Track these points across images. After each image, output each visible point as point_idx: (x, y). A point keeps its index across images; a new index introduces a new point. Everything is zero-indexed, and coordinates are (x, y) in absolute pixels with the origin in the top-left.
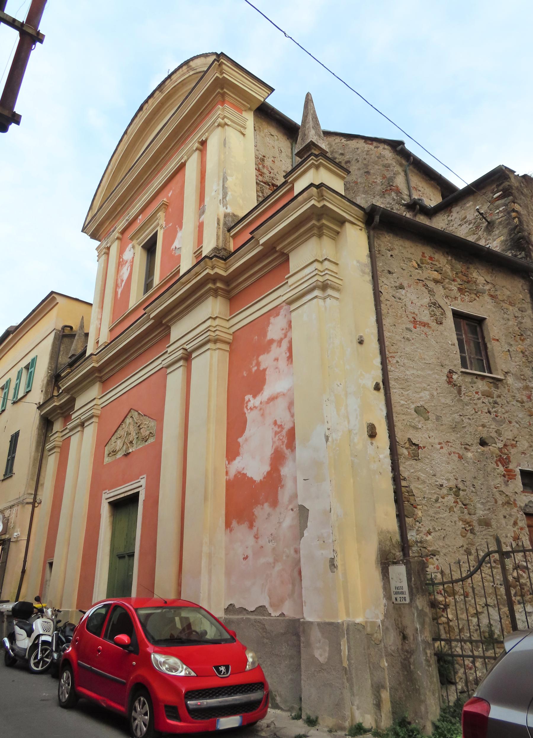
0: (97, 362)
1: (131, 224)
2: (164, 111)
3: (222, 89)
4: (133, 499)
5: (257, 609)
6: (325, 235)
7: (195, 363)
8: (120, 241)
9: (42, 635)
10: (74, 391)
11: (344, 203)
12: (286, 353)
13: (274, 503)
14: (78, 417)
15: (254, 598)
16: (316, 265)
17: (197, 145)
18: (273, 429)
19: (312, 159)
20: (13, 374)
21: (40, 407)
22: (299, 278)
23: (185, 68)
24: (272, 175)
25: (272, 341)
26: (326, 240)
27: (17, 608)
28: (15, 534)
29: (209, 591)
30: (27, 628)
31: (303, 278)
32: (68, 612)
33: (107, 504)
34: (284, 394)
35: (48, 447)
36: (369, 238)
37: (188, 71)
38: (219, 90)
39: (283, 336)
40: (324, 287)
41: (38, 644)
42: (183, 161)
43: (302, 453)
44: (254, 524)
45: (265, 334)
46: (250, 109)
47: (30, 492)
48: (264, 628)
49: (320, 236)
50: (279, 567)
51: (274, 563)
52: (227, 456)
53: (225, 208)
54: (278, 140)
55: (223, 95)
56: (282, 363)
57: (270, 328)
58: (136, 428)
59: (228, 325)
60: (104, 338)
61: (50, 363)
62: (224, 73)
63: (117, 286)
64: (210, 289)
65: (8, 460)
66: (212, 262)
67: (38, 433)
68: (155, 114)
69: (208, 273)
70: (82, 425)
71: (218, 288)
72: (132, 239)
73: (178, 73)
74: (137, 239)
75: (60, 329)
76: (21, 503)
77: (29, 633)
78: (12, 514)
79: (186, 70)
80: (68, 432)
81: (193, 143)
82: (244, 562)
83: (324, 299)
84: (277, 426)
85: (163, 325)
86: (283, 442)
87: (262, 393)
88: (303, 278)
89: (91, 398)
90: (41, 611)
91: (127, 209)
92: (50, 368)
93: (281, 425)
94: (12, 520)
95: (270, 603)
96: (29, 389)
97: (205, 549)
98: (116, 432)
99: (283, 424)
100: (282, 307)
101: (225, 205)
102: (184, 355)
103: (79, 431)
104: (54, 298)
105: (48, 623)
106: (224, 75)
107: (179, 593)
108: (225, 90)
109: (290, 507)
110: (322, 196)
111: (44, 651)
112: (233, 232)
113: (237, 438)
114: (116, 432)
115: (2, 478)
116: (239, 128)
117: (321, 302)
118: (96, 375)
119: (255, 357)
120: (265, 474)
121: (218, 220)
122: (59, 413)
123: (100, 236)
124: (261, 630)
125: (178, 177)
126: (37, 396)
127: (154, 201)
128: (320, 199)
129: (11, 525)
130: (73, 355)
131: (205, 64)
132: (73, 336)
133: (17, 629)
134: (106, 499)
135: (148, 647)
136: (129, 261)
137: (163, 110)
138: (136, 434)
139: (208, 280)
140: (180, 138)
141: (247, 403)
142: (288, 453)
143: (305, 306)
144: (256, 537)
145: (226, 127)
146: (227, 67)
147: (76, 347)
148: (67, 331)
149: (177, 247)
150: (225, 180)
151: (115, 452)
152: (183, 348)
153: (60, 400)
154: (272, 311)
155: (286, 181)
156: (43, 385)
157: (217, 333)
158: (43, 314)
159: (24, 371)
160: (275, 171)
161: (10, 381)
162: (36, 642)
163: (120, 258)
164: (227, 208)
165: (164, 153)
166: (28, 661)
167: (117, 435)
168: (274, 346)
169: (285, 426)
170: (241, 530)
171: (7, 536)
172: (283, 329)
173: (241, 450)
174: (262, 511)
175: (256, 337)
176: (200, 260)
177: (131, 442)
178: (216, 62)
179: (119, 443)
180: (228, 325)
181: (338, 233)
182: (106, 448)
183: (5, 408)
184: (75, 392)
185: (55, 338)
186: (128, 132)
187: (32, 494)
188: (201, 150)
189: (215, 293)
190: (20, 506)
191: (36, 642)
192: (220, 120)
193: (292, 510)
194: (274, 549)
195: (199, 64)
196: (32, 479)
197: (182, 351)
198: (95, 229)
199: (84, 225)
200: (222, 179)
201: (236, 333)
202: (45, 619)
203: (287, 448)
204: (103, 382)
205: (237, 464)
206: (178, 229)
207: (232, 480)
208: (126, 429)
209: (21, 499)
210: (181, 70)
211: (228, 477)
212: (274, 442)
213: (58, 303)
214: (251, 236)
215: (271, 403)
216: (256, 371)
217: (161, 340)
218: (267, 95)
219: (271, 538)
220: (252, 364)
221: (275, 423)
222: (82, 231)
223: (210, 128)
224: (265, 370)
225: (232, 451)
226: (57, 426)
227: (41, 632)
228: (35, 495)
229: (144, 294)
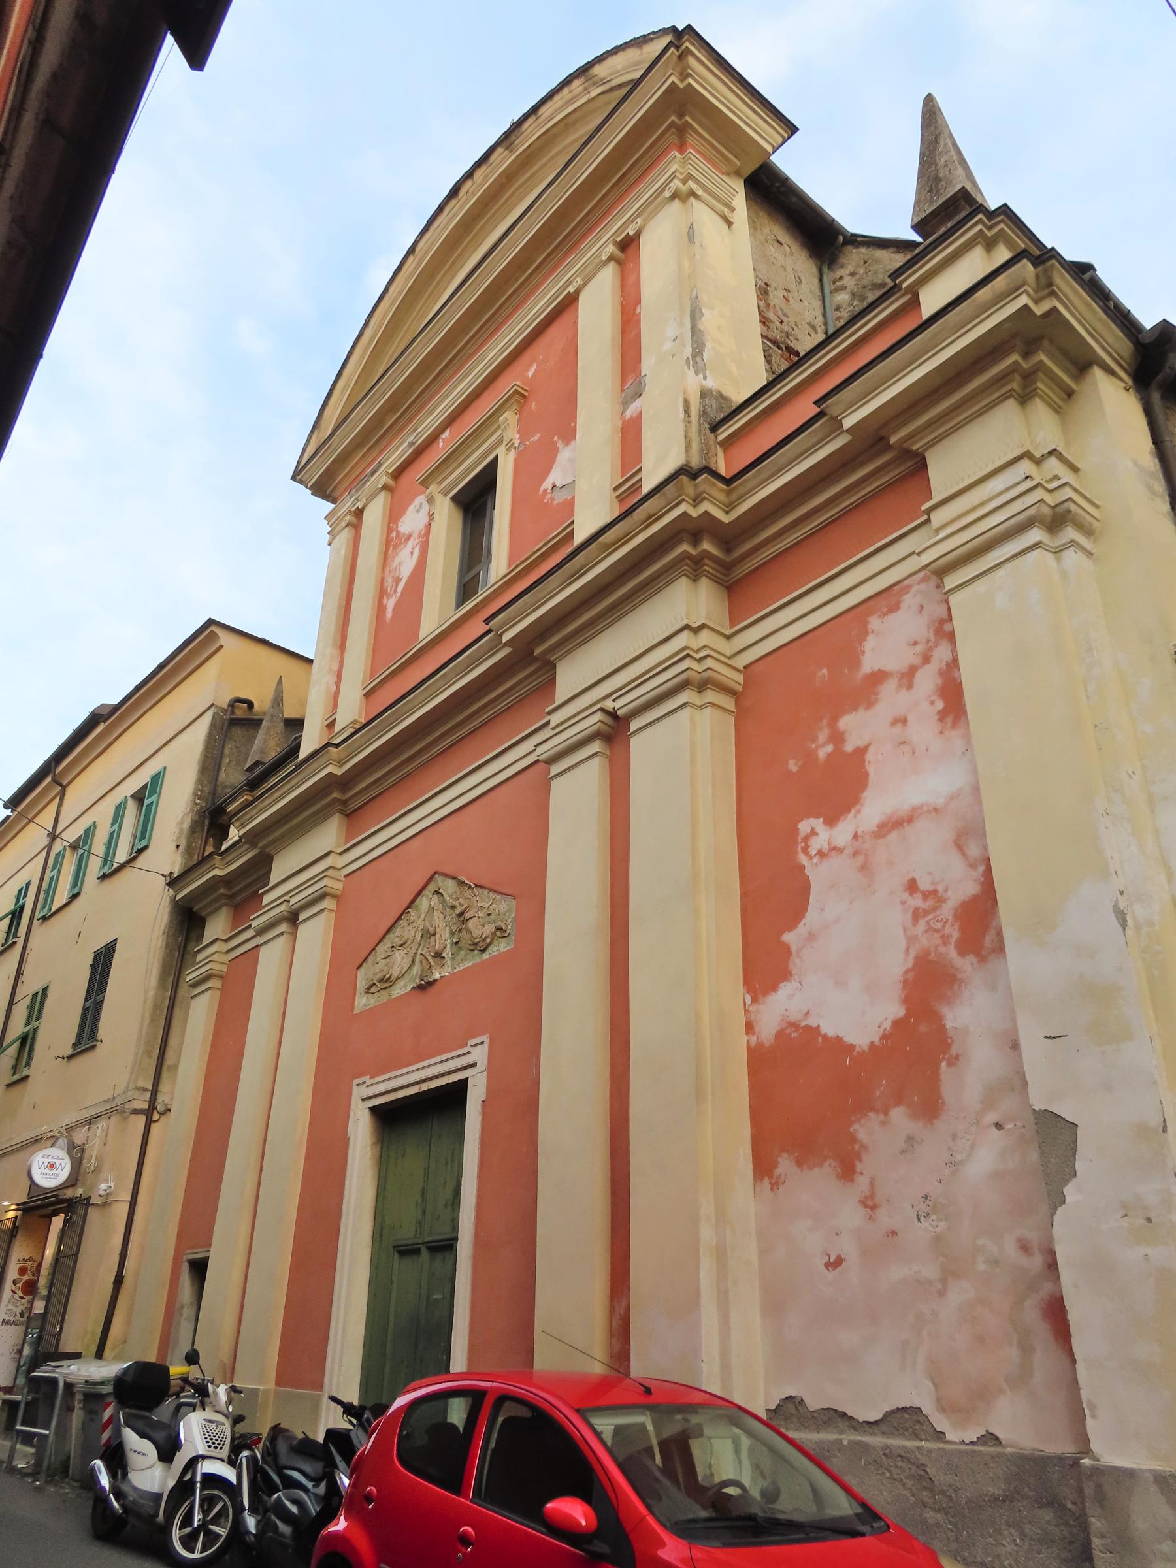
0: (341, 763)
1: (419, 453)
3: (681, 115)
4: (449, 1100)
5: (888, 1415)
6: (1041, 398)
7: (640, 746)
8: (389, 495)
9: (204, 1457)
10: (271, 838)
11: (1094, 312)
12: (932, 703)
13: (930, 1107)
14: (283, 899)
15: (875, 1381)
16: (1026, 466)
17: (611, 249)
18: (903, 903)
19: (980, 221)
20: (106, 810)
21: (174, 882)
22: (955, 515)
23: (576, 83)
24: (785, 327)
25: (879, 677)
26: (1040, 410)
27: (129, 1379)
28: (103, 1186)
29: (725, 1353)
30: (160, 1436)
31: (982, 504)
32: (255, 1392)
33: (367, 1113)
34: (936, 810)
35: (191, 976)
36: (1148, 412)
37: (585, 89)
38: (673, 118)
39: (917, 661)
40: (1057, 520)
41: (192, 1482)
42: (571, 289)
43: (1025, 961)
44: (859, 1167)
45: (855, 661)
46: (737, 173)
47: (141, 1084)
48: (923, 1479)
49: (1024, 400)
50: (960, 1294)
51: (944, 1281)
52: (748, 982)
53: (701, 376)
54: (791, 254)
55: (682, 131)
56: (924, 727)
57: (870, 643)
58: (452, 918)
59: (727, 648)
60: (351, 710)
61: (199, 782)
62: (689, 75)
63: (382, 593)
64: (685, 556)
65: (85, 1010)
66: (696, 486)
67: (167, 944)
68: (487, 205)
70: (293, 918)
71: (706, 554)
72: (425, 483)
73: (557, 98)
74: (440, 483)
75: (225, 706)
76: (117, 1110)
77: (168, 1450)
78: (95, 1139)
79: (581, 88)
80: (254, 937)
81: (603, 243)
82: (831, 1275)
83: (1058, 552)
84: (918, 896)
85: (536, 659)
86: (945, 939)
87: (859, 812)
88: (982, 504)
89: (316, 856)
90: (202, 1391)
91: (415, 415)
92: (199, 793)
93: (935, 892)
94: (93, 1151)
95: (938, 1400)
96: (144, 843)
97: (707, 1234)
98: (389, 931)
99: (940, 888)
100: (909, 587)
101: (700, 370)
102: (604, 727)
103: (282, 934)
104: (213, 636)
105: (218, 1423)
106: (690, 81)
107: (621, 1354)
108: (688, 118)
109: (991, 1117)
110: (1050, 284)
111: (208, 1503)
112: (725, 433)
113: (781, 933)
114: (389, 931)
115: (69, 1051)
116: (720, 207)
117: (1050, 558)
118: (335, 795)
119: (825, 722)
120: (887, 1025)
121: (687, 404)
122: (222, 894)
123: (335, 487)
124: (910, 1483)
125: (553, 331)
126: (166, 853)
127: (486, 394)
128: (1042, 294)
129: (89, 1164)
130: (257, 764)
131: (636, 64)
132: (257, 723)
133: (131, 1438)
134: (363, 1100)
135: (663, 1544)
136: (415, 535)
137: (511, 191)
138: (452, 934)
139: (679, 532)
140: (560, 243)
141: (806, 838)
142: (968, 968)
143: (1000, 573)
144: (870, 1204)
145: (692, 199)
146: (698, 64)
147: (266, 745)
148: (241, 711)
149: (559, 484)
150: (695, 315)
151: (387, 982)
152: (602, 709)
153: (229, 864)
154: (871, 603)
155: (895, 285)
156: (181, 832)
157: (709, 663)
158: (99, 751)
159: (131, 807)
160: (792, 319)
161: (95, 828)
162: (188, 1477)
163: (389, 530)
164: (705, 378)
165: (517, 280)
166: (166, 1529)
167: (394, 939)
168: (888, 689)
169: (949, 894)
170: (811, 1187)
171: (79, 1192)
172: (915, 643)
173: (795, 965)
174: (883, 1133)
175: (825, 671)
176: (631, 502)
177: (438, 955)
178: (672, 49)
179: (400, 960)
180: (727, 648)
181: (1070, 394)
182: (361, 973)
183: (81, 889)
184: (274, 841)
185: (213, 726)
186: (418, 249)
187: (146, 1090)
188: (619, 262)
189: (695, 568)
190: (115, 1119)
191: (188, 1477)
192: (676, 184)
193: (998, 1126)
194: (938, 1239)
195: (619, 67)
196: (148, 1053)
197: (599, 716)
198: (325, 472)
199: (298, 463)
200: (688, 313)
201: (753, 667)
202: (209, 1414)
203: (962, 953)
204: (348, 816)
205: (783, 1005)
206: (560, 444)
207: (767, 1044)
208: (420, 924)
209: (119, 1101)
210: (565, 91)
211: (754, 1039)
212: (911, 940)
213: (221, 647)
214: (817, 410)
215: (893, 836)
216: (829, 755)
217: (520, 701)
218: (780, 140)
219: (923, 1208)
220: (814, 739)
221: (912, 886)
222: (293, 478)
224: (861, 752)
225: (764, 967)
226: (217, 927)
227: (202, 1449)
228: (154, 1092)
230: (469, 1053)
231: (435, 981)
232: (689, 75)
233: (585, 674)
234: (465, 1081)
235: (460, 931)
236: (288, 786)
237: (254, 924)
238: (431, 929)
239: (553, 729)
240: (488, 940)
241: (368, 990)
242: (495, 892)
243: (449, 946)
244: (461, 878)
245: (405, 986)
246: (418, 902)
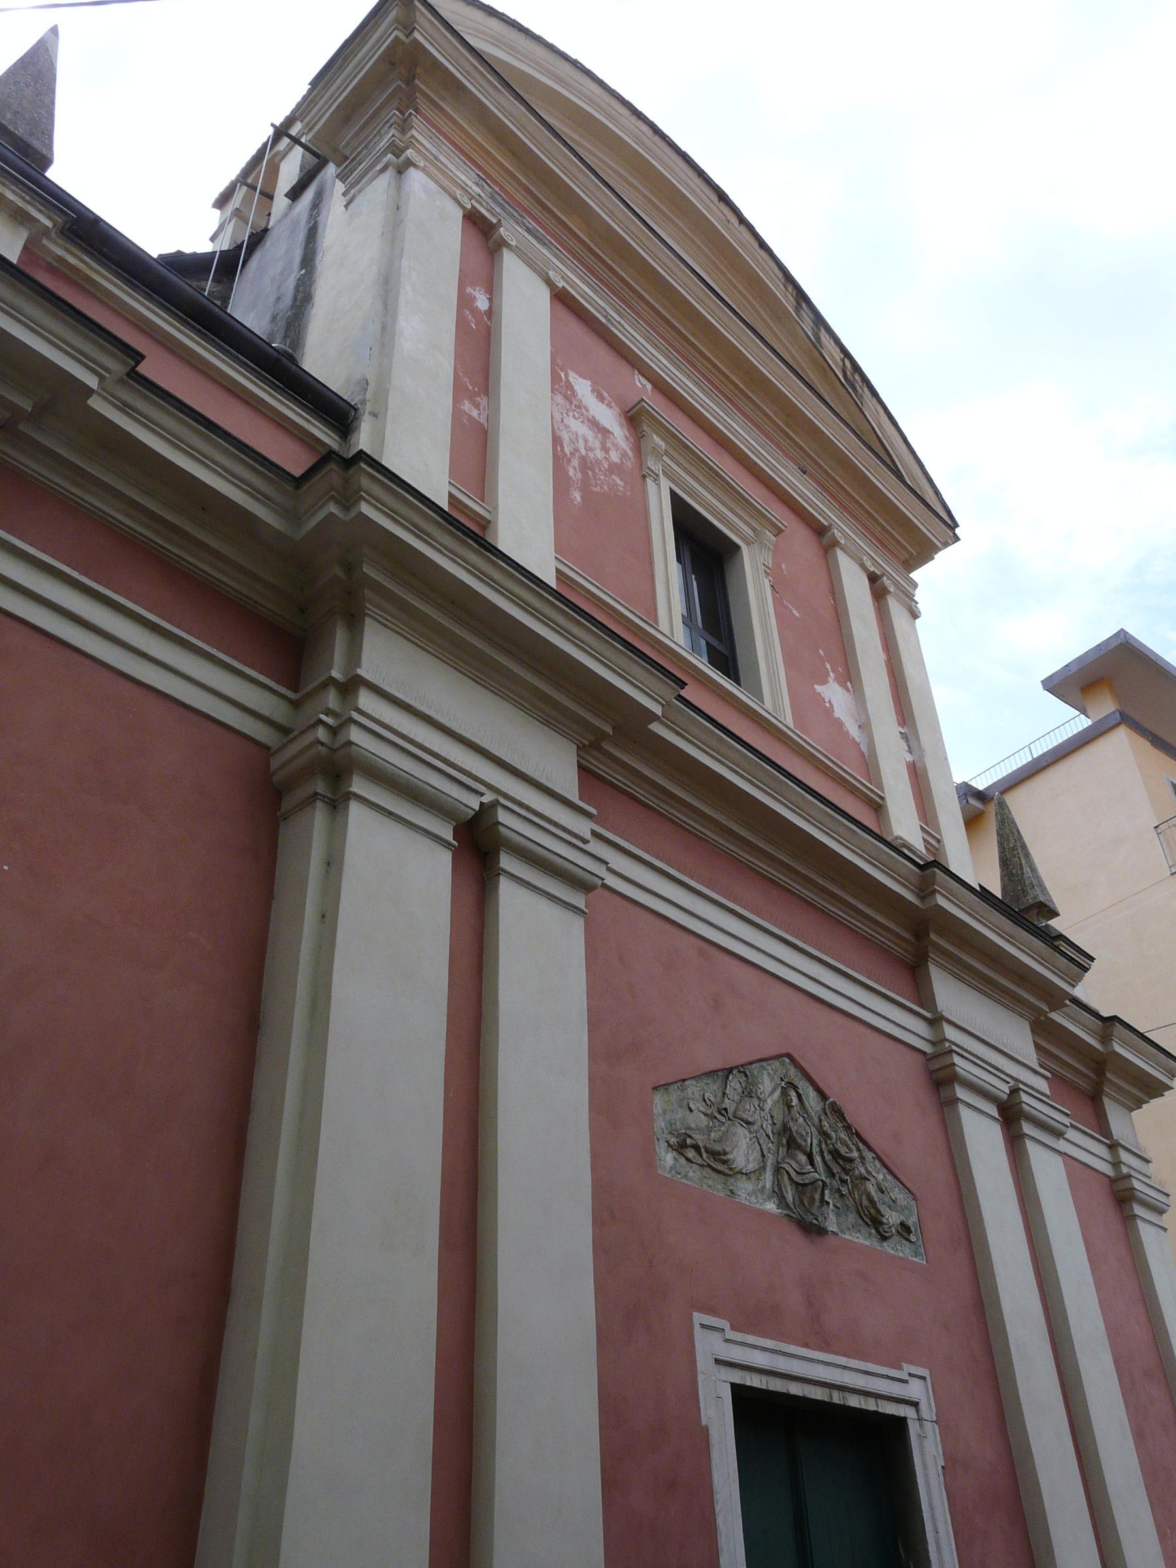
230: (906, 1382)
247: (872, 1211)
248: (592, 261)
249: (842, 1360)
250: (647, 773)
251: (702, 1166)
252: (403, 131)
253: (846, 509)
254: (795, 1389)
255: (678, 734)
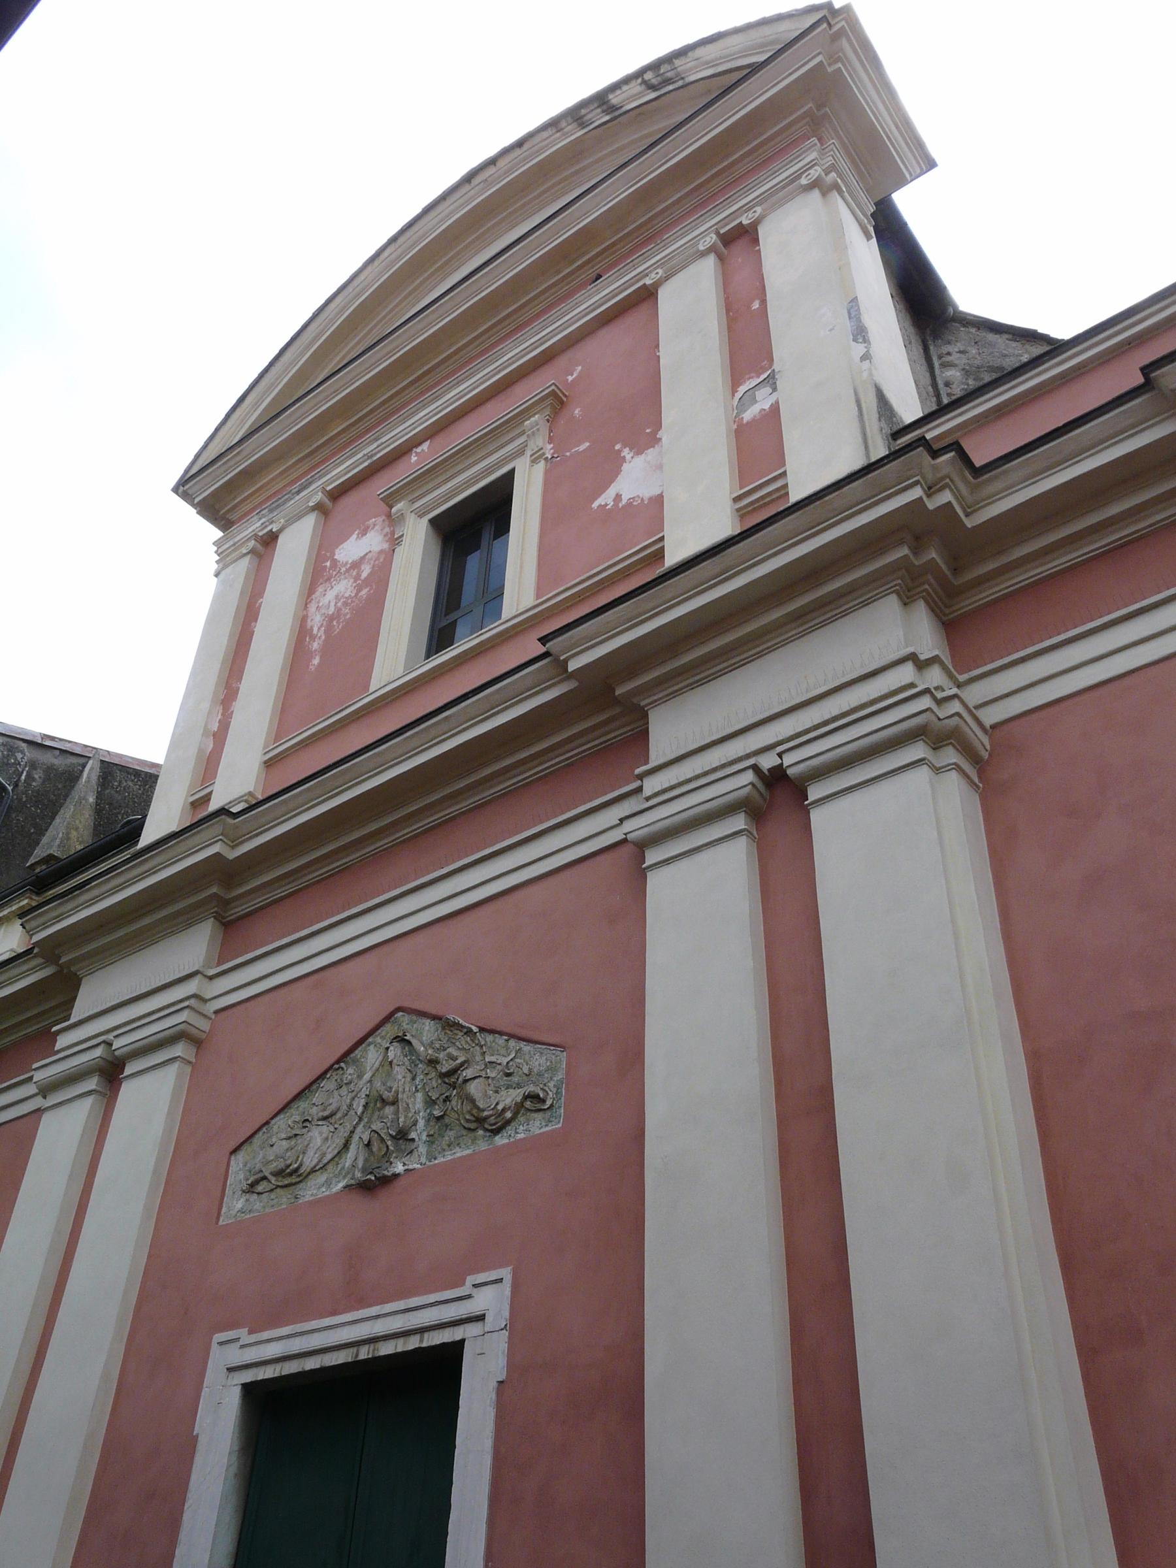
2: (596, 162)
17: (712, 238)
69: (218, 854)
70: (112, 1073)
74: (413, 501)
85: (616, 701)
98: (297, 1097)
134: (230, 1370)
138: (430, 1103)
145: (835, 193)
151: (291, 1176)
167: (311, 1107)
176: (766, 517)
177: (402, 1136)
182: (237, 1162)
184: (84, 957)
188: (721, 258)
198: (223, 487)
199: (186, 472)
206: (626, 453)
222: (175, 490)
223: (771, 195)
229: (428, 656)
230: (469, 1297)
231: (396, 1176)
232: (839, 60)
233: (700, 731)
234: (457, 1347)
235: (447, 1099)
236: (135, 872)
237: (38, 1076)
238: (386, 1095)
239: (648, 799)
240: (508, 1115)
241: (251, 1188)
242: (523, 1040)
243: (421, 1123)
244: (450, 1017)
245: (328, 1183)
246: (358, 1053)
247: (475, 1112)
248: (362, 426)
249: (328, 1321)
250: (266, 880)
251: (272, 1190)
252: (820, 106)
253: (713, 197)
254: (312, 1364)
255: (257, 835)
